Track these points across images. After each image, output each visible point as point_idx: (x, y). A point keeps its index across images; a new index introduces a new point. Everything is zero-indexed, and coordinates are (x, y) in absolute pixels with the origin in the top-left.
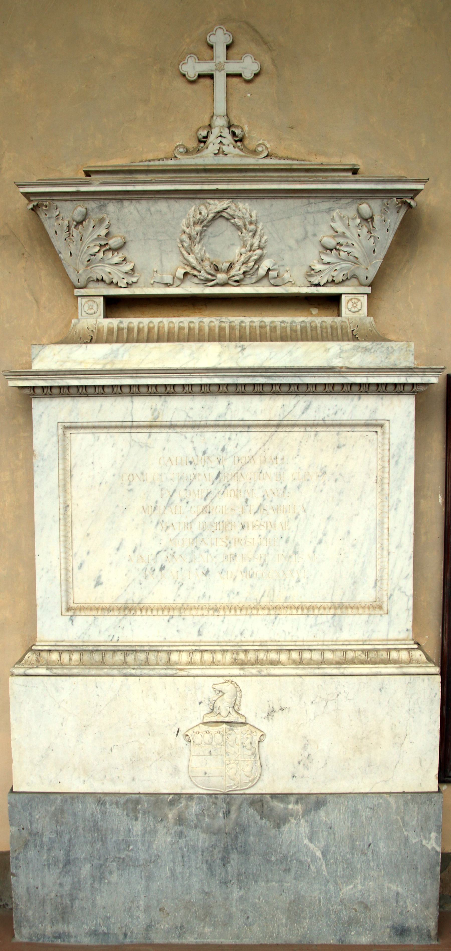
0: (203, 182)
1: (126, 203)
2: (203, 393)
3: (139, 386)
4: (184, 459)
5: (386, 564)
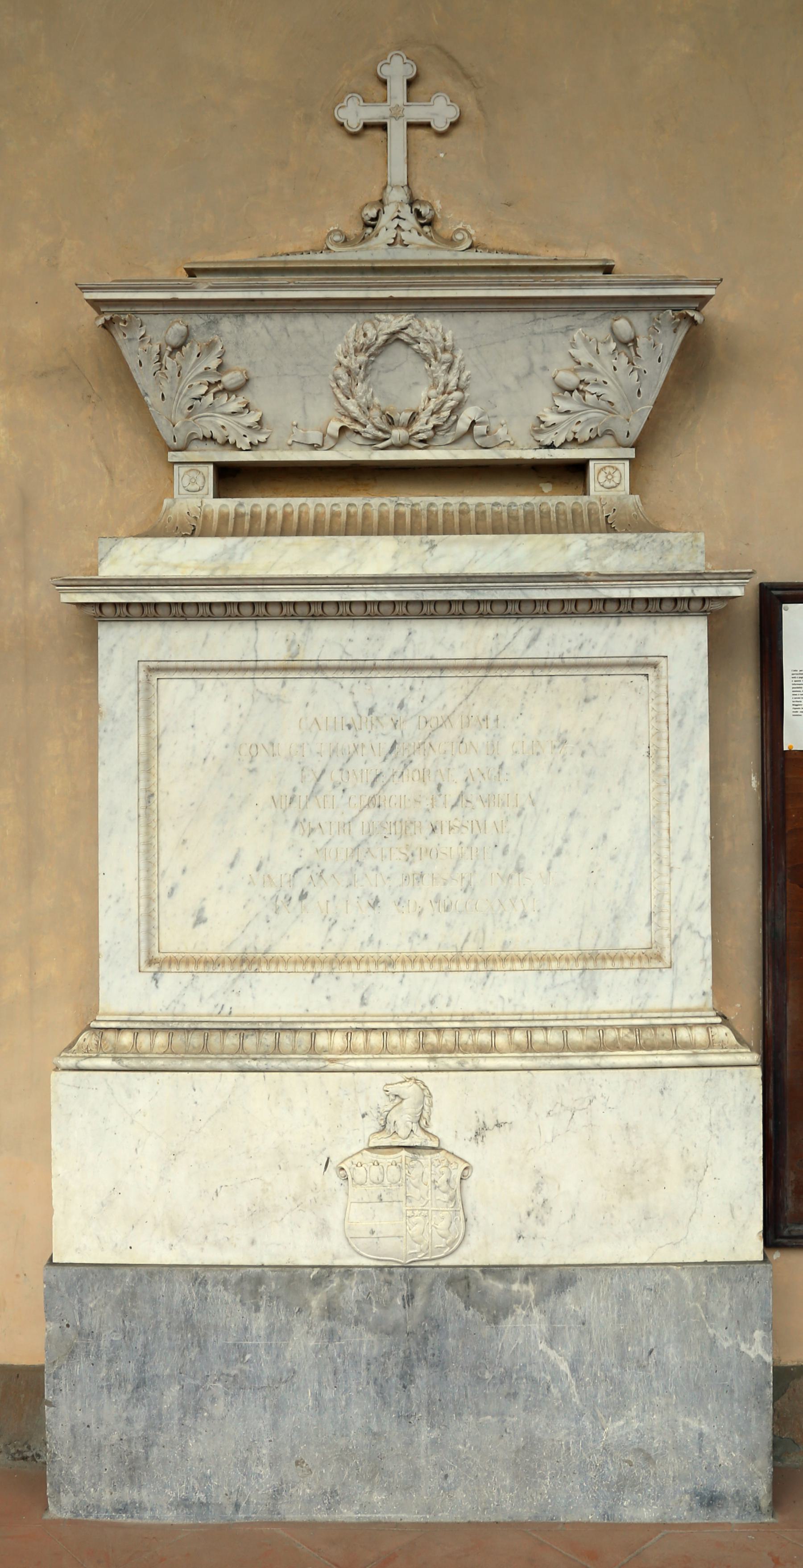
0: (369, 287)
1: (249, 319)
2: (369, 615)
3: (267, 604)
4: (339, 720)
5: (667, 886)
